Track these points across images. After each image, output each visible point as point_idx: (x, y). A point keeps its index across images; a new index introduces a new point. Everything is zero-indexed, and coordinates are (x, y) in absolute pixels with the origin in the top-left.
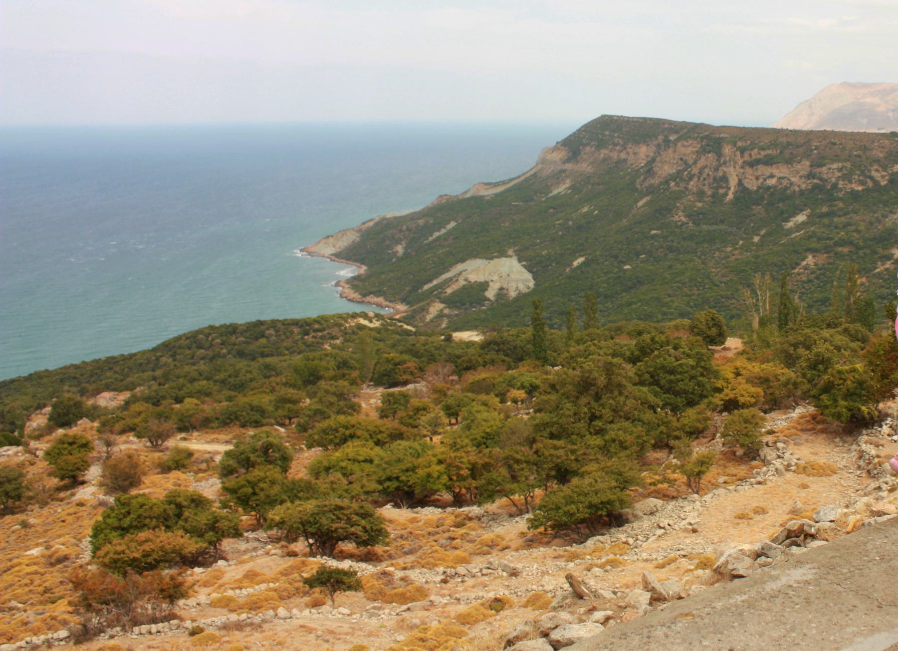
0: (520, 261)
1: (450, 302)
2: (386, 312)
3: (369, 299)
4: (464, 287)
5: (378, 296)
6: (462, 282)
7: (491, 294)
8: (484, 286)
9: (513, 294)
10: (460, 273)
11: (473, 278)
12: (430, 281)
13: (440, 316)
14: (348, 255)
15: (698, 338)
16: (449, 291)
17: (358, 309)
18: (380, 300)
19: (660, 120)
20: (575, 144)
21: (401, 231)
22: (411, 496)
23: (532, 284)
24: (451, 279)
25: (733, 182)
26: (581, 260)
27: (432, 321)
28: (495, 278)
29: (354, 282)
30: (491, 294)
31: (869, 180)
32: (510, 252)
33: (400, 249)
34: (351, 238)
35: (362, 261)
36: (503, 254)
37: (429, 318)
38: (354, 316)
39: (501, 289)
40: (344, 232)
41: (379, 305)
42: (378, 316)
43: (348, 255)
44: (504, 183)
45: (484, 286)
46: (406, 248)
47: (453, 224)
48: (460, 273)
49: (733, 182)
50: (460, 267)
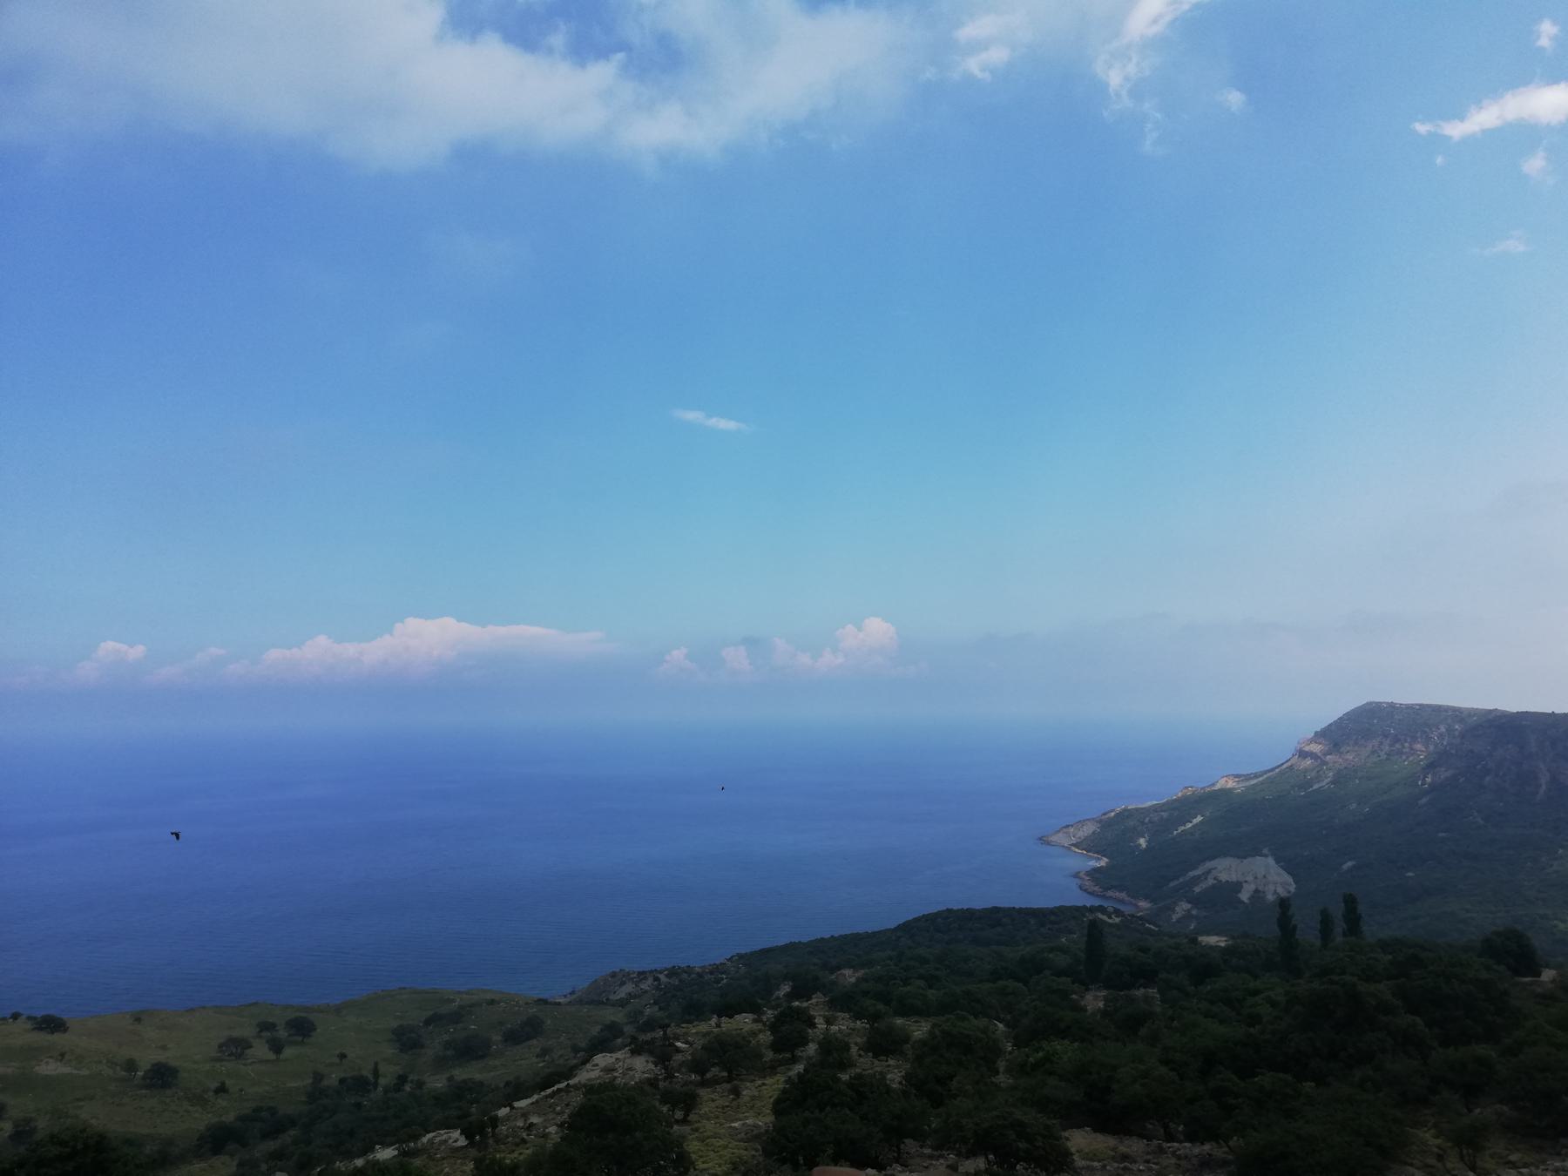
0: (1277, 862)
1: (1195, 901)
2: (1127, 910)
3: (1110, 893)
4: (1214, 886)
5: (1121, 891)
6: (1211, 882)
7: (1244, 896)
8: (1238, 886)
9: (1270, 897)
10: (1209, 872)
11: (1224, 877)
12: (1195, 868)
13: (1188, 916)
14: (1090, 846)
15: (702, 1166)
16: (1197, 889)
17: (1097, 902)
18: (1123, 895)
19: (1439, 707)
20: (1339, 734)
21: (1143, 823)
22: (1110, 1116)
23: (1292, 888)
24: (1199, 877)
25: (1544, 779)
26: (1350, 864)
27: (1178, 921)
28: (1250, 878)
29: (1094, 874)
30: (1244, 896)
31: (1058, 1045)
32: (1265, 851)
33: (1142, 842)
34: (1089, 829)
35: (1103, 853)
36: (1257, 852)
37: (1175, 918)
38: (1092, 910)
39: (1257, 891)
40: (1082, 822)
41: (1122, 901)
42: (1118, 912)
43: (1090, 846)
44: (1256, 776)
45: (1238, 886)
46: (1148, 842)
47: (1199, 818)
48: (1209, 872)
49: (1544, 779)
50: (1209, 865)
